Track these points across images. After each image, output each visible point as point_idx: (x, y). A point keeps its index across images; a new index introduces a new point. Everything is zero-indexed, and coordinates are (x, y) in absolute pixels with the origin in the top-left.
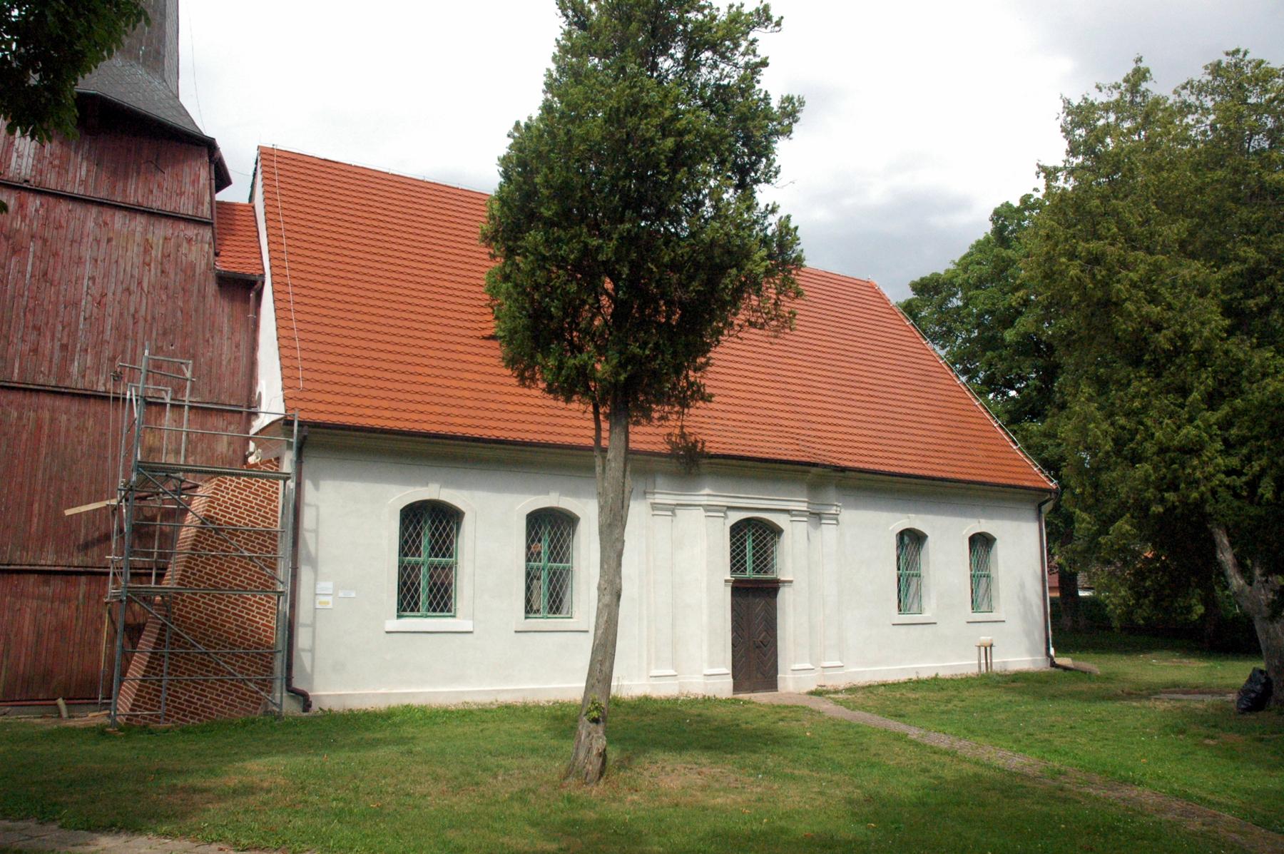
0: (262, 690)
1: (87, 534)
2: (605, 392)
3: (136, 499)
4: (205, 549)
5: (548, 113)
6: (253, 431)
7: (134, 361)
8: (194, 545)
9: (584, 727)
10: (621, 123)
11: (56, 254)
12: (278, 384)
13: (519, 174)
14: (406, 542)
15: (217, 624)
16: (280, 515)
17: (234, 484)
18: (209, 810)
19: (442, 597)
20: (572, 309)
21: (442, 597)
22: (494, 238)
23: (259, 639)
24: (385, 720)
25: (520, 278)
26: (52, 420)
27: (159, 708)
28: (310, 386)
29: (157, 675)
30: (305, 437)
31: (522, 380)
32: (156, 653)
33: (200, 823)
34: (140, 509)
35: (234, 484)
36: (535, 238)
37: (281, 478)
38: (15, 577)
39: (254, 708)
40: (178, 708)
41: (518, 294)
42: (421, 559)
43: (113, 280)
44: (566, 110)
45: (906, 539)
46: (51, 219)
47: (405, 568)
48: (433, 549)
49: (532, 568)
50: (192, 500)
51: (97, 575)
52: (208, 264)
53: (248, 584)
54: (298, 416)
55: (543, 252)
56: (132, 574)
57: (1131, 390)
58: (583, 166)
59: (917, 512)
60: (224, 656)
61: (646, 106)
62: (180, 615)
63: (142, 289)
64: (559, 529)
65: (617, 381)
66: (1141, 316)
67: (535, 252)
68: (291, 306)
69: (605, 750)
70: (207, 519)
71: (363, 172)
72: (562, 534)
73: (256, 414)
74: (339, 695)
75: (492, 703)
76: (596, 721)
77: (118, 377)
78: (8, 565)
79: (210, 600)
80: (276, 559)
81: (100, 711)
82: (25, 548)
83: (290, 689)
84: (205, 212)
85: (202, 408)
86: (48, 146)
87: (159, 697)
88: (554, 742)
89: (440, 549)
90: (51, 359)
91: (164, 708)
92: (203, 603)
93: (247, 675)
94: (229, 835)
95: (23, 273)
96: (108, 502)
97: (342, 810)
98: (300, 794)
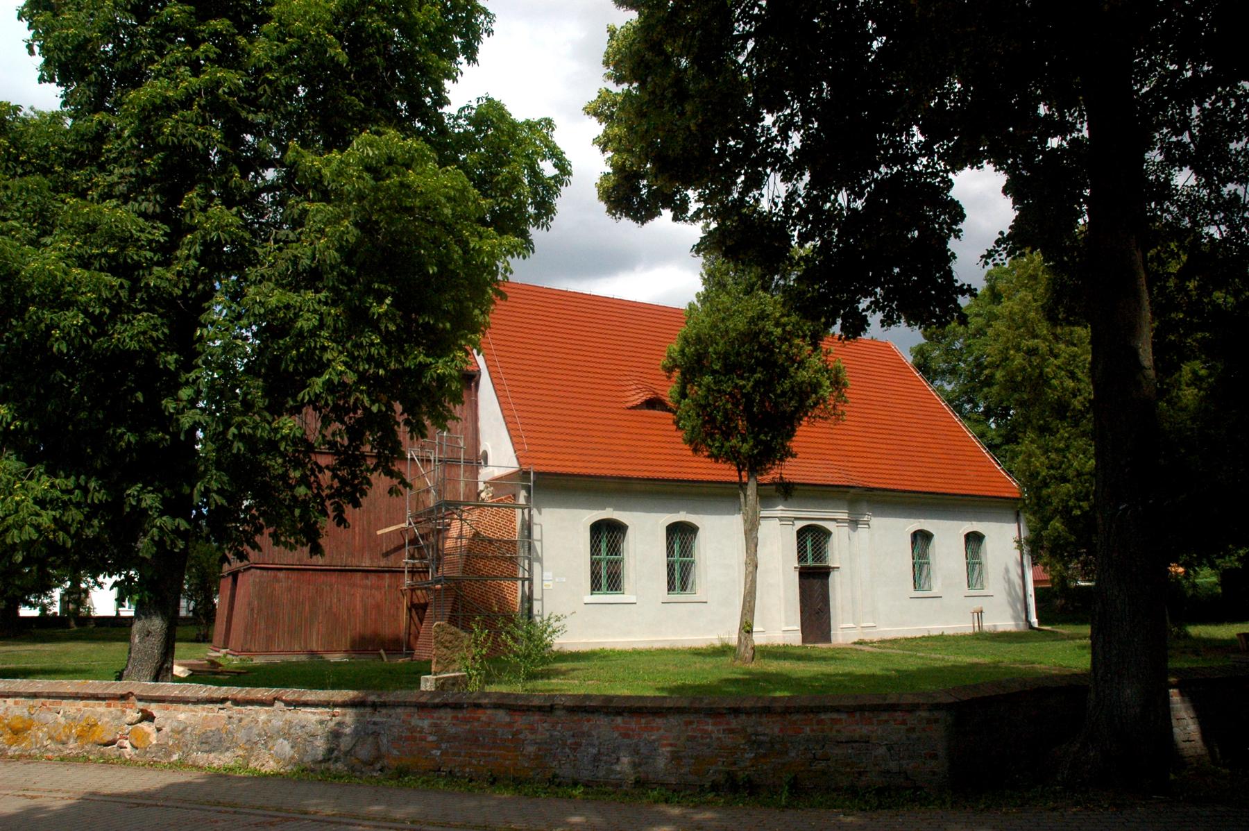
31: (695, 450)
45: (918, 537)
51: (396, 572)
54: (532, 469)
57: (1058, 436)
59: (925, 518)
66: (1063, 388)
82: (353, 556)
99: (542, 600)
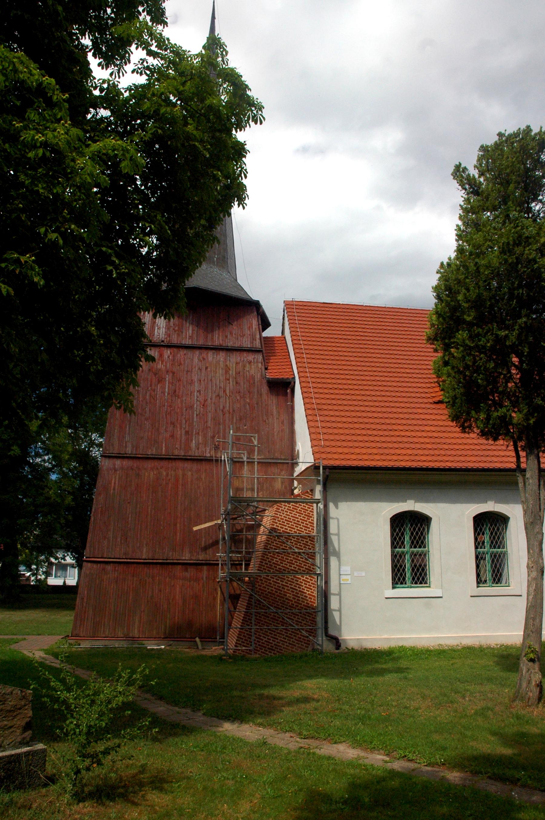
0: (310, 635)
1: (205, 542)
2: (521, 432)
3: (231, 519)
4: (272, 548)
5: (461, 253)
6: (296, 474)
7: (224, 438)
8: (265, 546)
9: (524, 665)
10: (511, 252)
11: (179, 380)
12: (309, 444)
13: (447, 296)
14: (395, 539)
15: (282, 594)
16: (315, 525)
17: (287, 508)
18: (283, 711)
19: (421, 574)
20: (492, 379)
21: (421, 574)
22: (435, 339)
23: (307, 603)
24: (387, 656)
25: (454, 362)
26: (184, 475)
27: (251, 645)
28: (328, 443)
29: (248, 625)
30: (328, 476)
32: (248, 612)
33: (278, 719)
34: (234, 525)
35: (287, 508)
36: (463, 336)
37: (314, 502)
38: (170, 566)
39: (306, 646)
40: (262, 646)
41: (455, 373)
42: (406, 550)
43: (210, 391)
44: (473, 250)
46: (176, 360)
47: (396, 556)
48: (412, 542)
49: (479, 553)
50: (263, 518)
51: (212, 565)
52: (261, 375)
53: (298, 569)
54: (322, 463)
55: (469, 344)
56: (231, 564)
58: (489, 284)
60: (287, 614)
61: (527, 238)
62: (260, 589)
63: (226, 395)
64: (496, 525)
65: (529, 424)
67: (465, 346)
68: (312, 395)
69: (541, 682)
70: (273, 530)
71: (348, 307)
72: (498, 529)
73: (297, 464)
74: (358, 639)
75: (458, 645)
76: (532, 660)
77: (217, 448)
78: (167, 560)
79: (276, 579)
80: (314, 553)
81: (218, 646)
83: (327, 635)
84: (257, 344)
85: (265, 463)
86: (172, 320)
87: (250, 639)
88: (504, 674)
89: (417, 542)
90: (181, 440)
91: (254, 645)
92: (273, 581)
93: (301, 626)
94: (295, 727)
95: (164, 393)
96: (216, 522)
97: (364, 716)
98: (337, 704)
99: (339, 594)
